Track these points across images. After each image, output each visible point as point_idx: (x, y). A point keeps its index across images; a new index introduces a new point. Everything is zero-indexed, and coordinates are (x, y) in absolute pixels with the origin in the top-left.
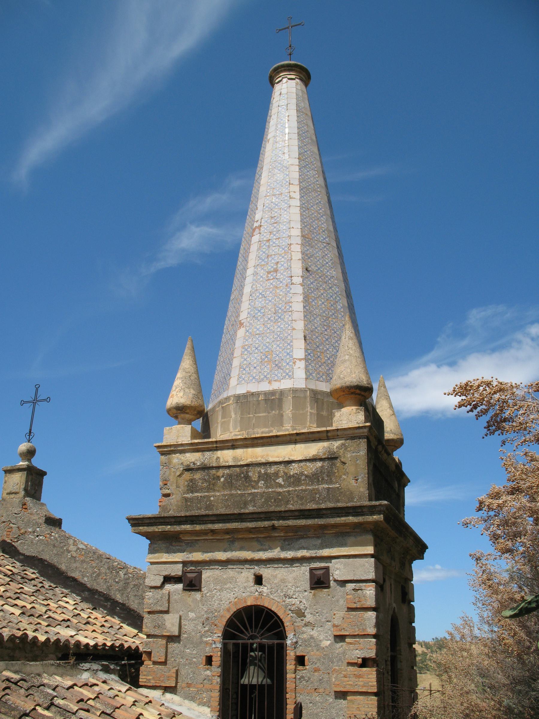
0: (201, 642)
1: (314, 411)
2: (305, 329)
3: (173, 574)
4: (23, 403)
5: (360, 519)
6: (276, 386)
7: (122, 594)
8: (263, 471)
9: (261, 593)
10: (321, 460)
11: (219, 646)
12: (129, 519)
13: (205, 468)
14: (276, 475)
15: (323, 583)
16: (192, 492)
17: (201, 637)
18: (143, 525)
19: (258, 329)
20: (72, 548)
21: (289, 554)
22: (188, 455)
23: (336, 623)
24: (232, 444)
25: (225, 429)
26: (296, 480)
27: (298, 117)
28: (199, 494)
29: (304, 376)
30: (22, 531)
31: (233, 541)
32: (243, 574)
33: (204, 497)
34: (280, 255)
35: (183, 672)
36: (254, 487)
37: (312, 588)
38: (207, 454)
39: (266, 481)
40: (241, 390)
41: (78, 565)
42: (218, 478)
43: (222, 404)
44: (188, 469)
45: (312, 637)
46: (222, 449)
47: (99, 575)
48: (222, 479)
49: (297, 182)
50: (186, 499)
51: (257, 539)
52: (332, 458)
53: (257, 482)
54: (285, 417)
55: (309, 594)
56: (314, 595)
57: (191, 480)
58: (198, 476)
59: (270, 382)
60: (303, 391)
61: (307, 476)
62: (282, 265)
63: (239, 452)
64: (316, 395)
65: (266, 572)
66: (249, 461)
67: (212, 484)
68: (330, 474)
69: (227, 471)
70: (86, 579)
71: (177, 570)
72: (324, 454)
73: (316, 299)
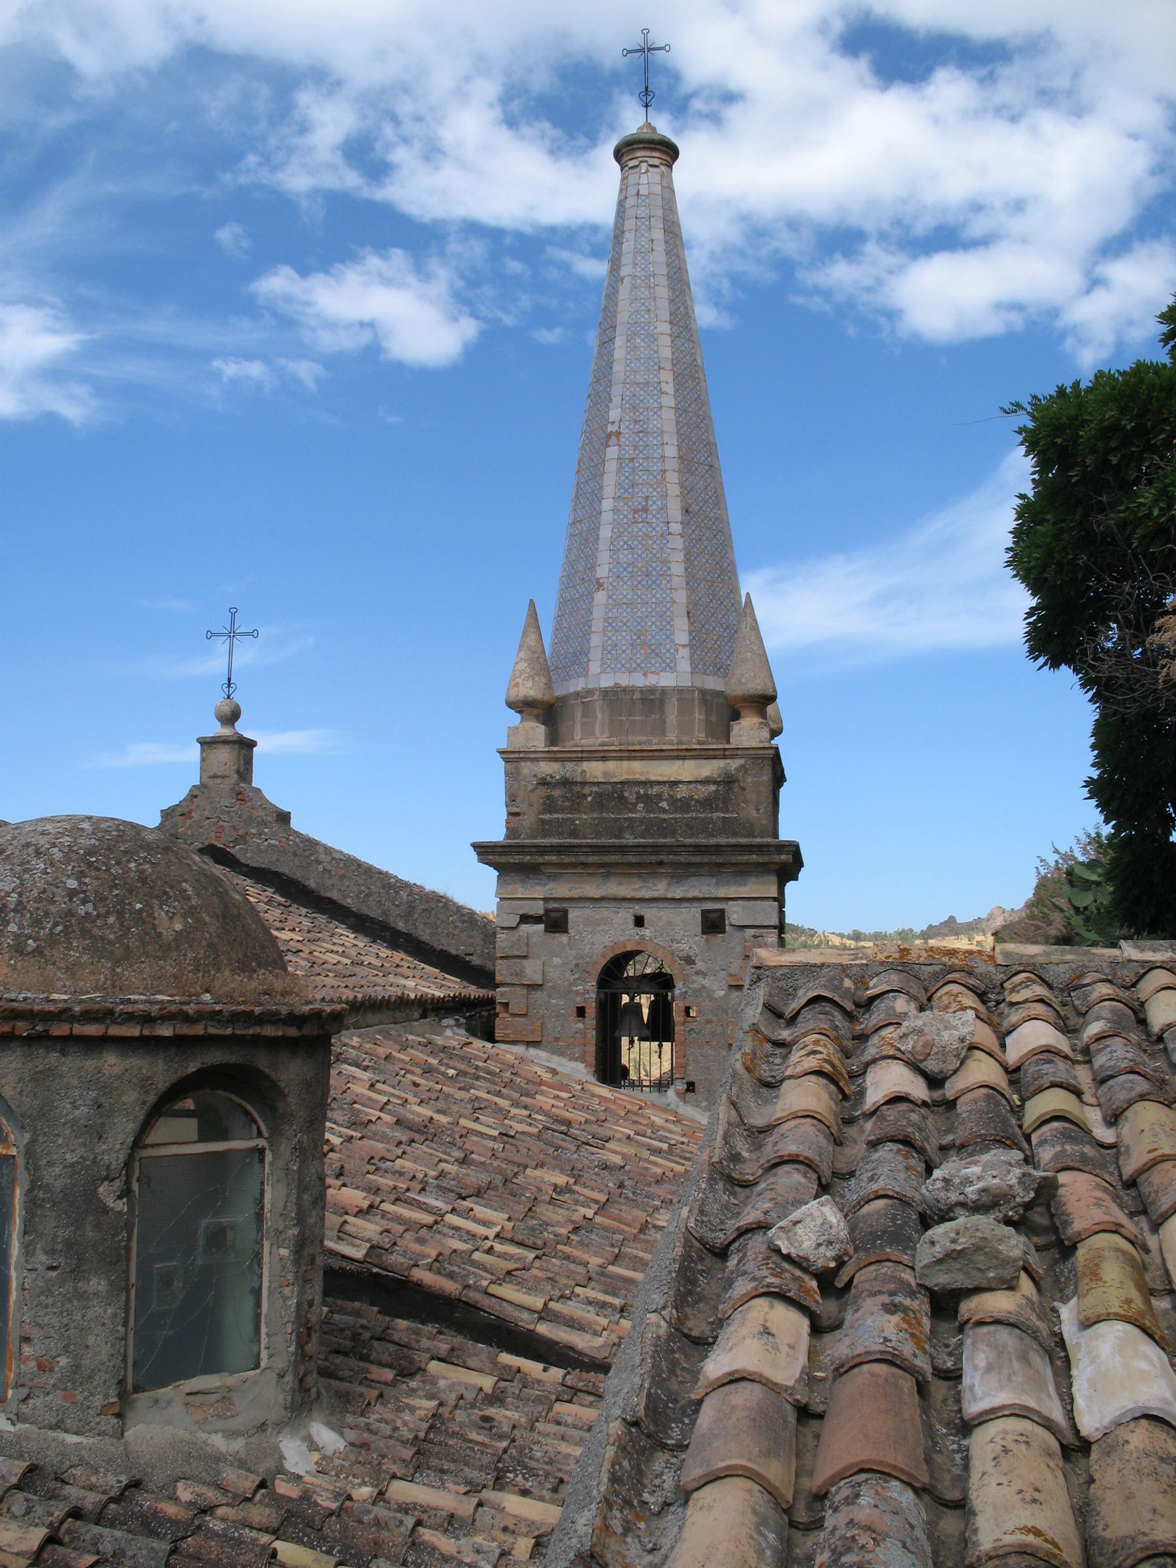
0: (570, 992)
1: (703, 717)
2: (688, 603)
3: (531, 913)
4: (211, 635)
5: (765, 859)
6: (652, 680)
7: (406, 922)
8: (642, 791)
9: (643, 937)
10: (715, 782)
11: (594, 996)
12: (475, 846)
13: (566, 783)
14: (659, 797)
15: (717, 927)
16: (550, 813)
17: (570, 985)
18: (493, 853)
19: (625, 596)
20: (323, 857)
21: (678, 892)
22: (543, 764)
23: (732, 971)
24: (603, 756)
25: (588, 731)
26: (683, 805)
27: (666, 242)
28: (560, 816)
29: (689, 669)
30: (241, 832)
31: (607, 876)
32: (620, 915)
33: (567, 820)
34: (651, 486)
35: (549, 1025)
36: (631, 811)
37: (704, 933)
38: (569, 766)
39: (646, 803)
40: (607, 682)
41: (335, 881)
42: (585, 796)
43: (582, 697)
44: (543, 783)
45: (703, 987)
46: (589, 760)
47: (368, 895)
48: (589, 799)
49: (668, 366)
50: (543, 822)
51: (639, 875)
52: (728, 781)
53: (635, 805)
54: (668, 724)
55: (701, 939)
56: (707, 940)
57: (548, 797)
58: (556, 792)
59: (645, 674)
60: (691, 690)
61: (697, 801)
62: (654, 503)
63: (611, 765)
64: (707, 697)
65: (648, 913)
66: (625, 777)
67: (576, 802)
68: (726, 801)
69: (595, 789)
70: (349, 900)
71: (538, 909)
72: (720, 776)
73: (698, 555)
